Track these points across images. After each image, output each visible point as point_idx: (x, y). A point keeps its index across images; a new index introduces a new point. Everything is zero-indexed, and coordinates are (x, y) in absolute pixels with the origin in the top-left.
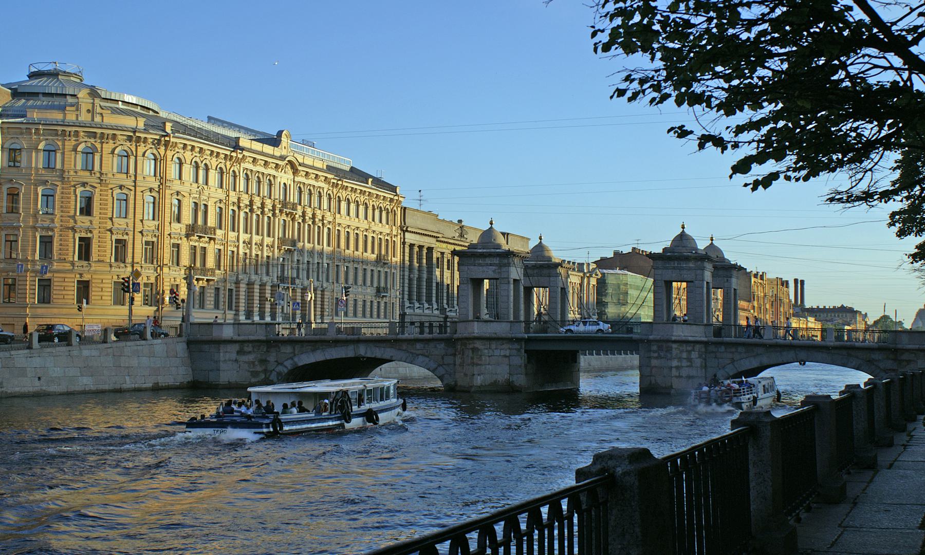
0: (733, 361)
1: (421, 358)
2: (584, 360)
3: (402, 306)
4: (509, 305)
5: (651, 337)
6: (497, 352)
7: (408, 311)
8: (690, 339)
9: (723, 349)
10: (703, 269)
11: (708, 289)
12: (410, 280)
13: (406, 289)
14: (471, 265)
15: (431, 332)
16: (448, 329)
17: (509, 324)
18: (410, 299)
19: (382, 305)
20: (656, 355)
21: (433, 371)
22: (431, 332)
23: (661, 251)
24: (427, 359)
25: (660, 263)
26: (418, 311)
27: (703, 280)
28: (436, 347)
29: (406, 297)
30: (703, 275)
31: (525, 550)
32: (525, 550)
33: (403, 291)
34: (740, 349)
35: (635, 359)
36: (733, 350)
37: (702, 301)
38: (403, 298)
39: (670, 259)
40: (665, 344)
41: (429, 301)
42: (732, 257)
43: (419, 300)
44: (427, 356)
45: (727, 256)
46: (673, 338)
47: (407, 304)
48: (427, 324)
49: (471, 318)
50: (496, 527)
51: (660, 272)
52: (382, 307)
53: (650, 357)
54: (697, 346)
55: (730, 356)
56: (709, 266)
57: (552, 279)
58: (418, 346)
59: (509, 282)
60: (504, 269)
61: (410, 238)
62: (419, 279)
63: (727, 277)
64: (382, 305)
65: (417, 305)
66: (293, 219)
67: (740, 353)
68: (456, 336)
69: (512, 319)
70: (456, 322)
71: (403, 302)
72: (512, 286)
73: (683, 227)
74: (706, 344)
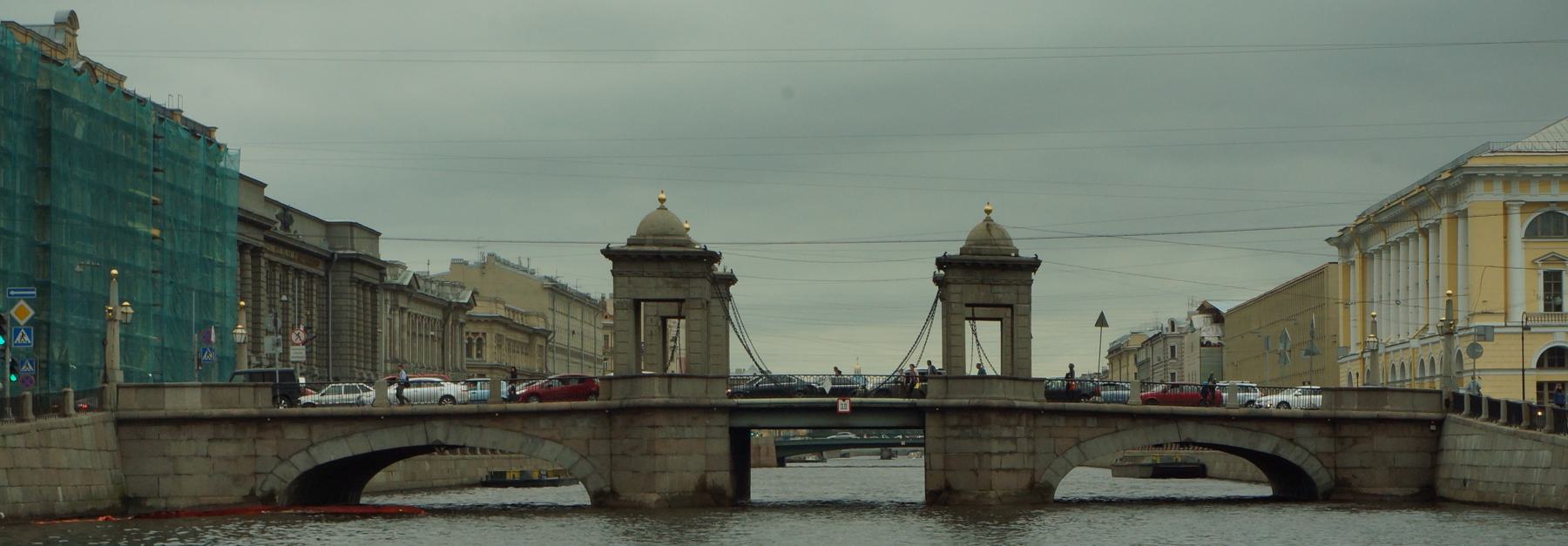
6: (688, 432)
9: (1061, 422)
24: (559, 448)
34: (1091, 422)
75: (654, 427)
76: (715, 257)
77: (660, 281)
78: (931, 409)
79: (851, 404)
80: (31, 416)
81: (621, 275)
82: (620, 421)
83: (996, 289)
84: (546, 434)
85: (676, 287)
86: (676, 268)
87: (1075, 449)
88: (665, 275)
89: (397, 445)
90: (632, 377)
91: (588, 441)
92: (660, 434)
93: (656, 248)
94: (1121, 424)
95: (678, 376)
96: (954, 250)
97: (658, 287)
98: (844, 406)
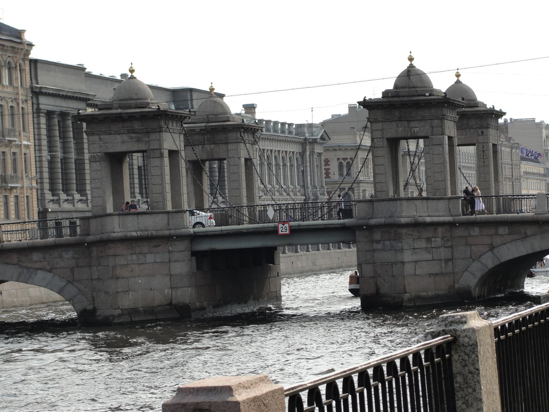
0: (492, 247)
1: (41, 274)
2: (285, 260)
3: (41, 200)
4: (163, 188)
5: (373, 222)
6: (150, 258)
7: (51, 207)
8: (428, 219)
9: (476, 231)
10: (442, 118)
11: (451, 146)
12: (51, 162)
13: (46, 175)
14: (105, 133)
15: (59, 234)
16: (78, 229)
17: (165, 216)
18: (53, 190)
19: (12, 200)
20: (380, 246)
21: (60, 292)
22: (59, 234)
23: (379, 96)
24: (50, 275)
25: (379, 114)
26: (66, 206)
27: (443, 134)
28: (61, 257)
29: (47, 186)
30: (442, 126)
31: (382, 408)
32: (382, 408)
33: (41, 178)
34: (503, 230)
35: (350, 254)
36: (492, 231)
37: (444, 163)
38: (42, 189)
39: (404, 105)
40: (393, 228)
41: (81, 190)
42: (487, 97)
43: (66, 190)
44: (50, 271)
45: (480, 98)
46: (403, 220)
47: (49, 196)
48: (66, 223)
49: (110, 209)
50: (409, 357)
51: (379, 126)
52: (12, 204)
53: (374, 251)
54: (440, 230)
55: (487, 240)
56: (452, 115)
57: (230, 146)
58: (36, 256)
59: (162, 156)
60: (153, 136)
61: (46, 103)
62: (65, 161)
63: (481, 128)
64: (12, 200)
65: (63, 196)
66: (18, 104)
67: (502, 235)
68: (90, 238)
69: (449, 195)
70: (88, 218)
71: (43, 194)
72: (166, 160)
73: (411, 59)
74: (451, 225)
75: (115, 256)
76: (501, 114)
77: (125, 137)
78: (360, 227)
79: (290, 227)
80: (331, 248)
81: (92, 134)
82: (95, 251)
83: (412, 124)
84: (38, 265)
85: (138, 140)
86: (137, 125)
87: (490, 254)
88: (129, 132)
89: (516, 255)
90: (101, 216)
91: (72, 270)
92: (120, 261)
93: (120, 111)
94: (530, 230)
95: (173, 212)
96: (375, 93)
97: (123, 142)
98: (284, 229)
